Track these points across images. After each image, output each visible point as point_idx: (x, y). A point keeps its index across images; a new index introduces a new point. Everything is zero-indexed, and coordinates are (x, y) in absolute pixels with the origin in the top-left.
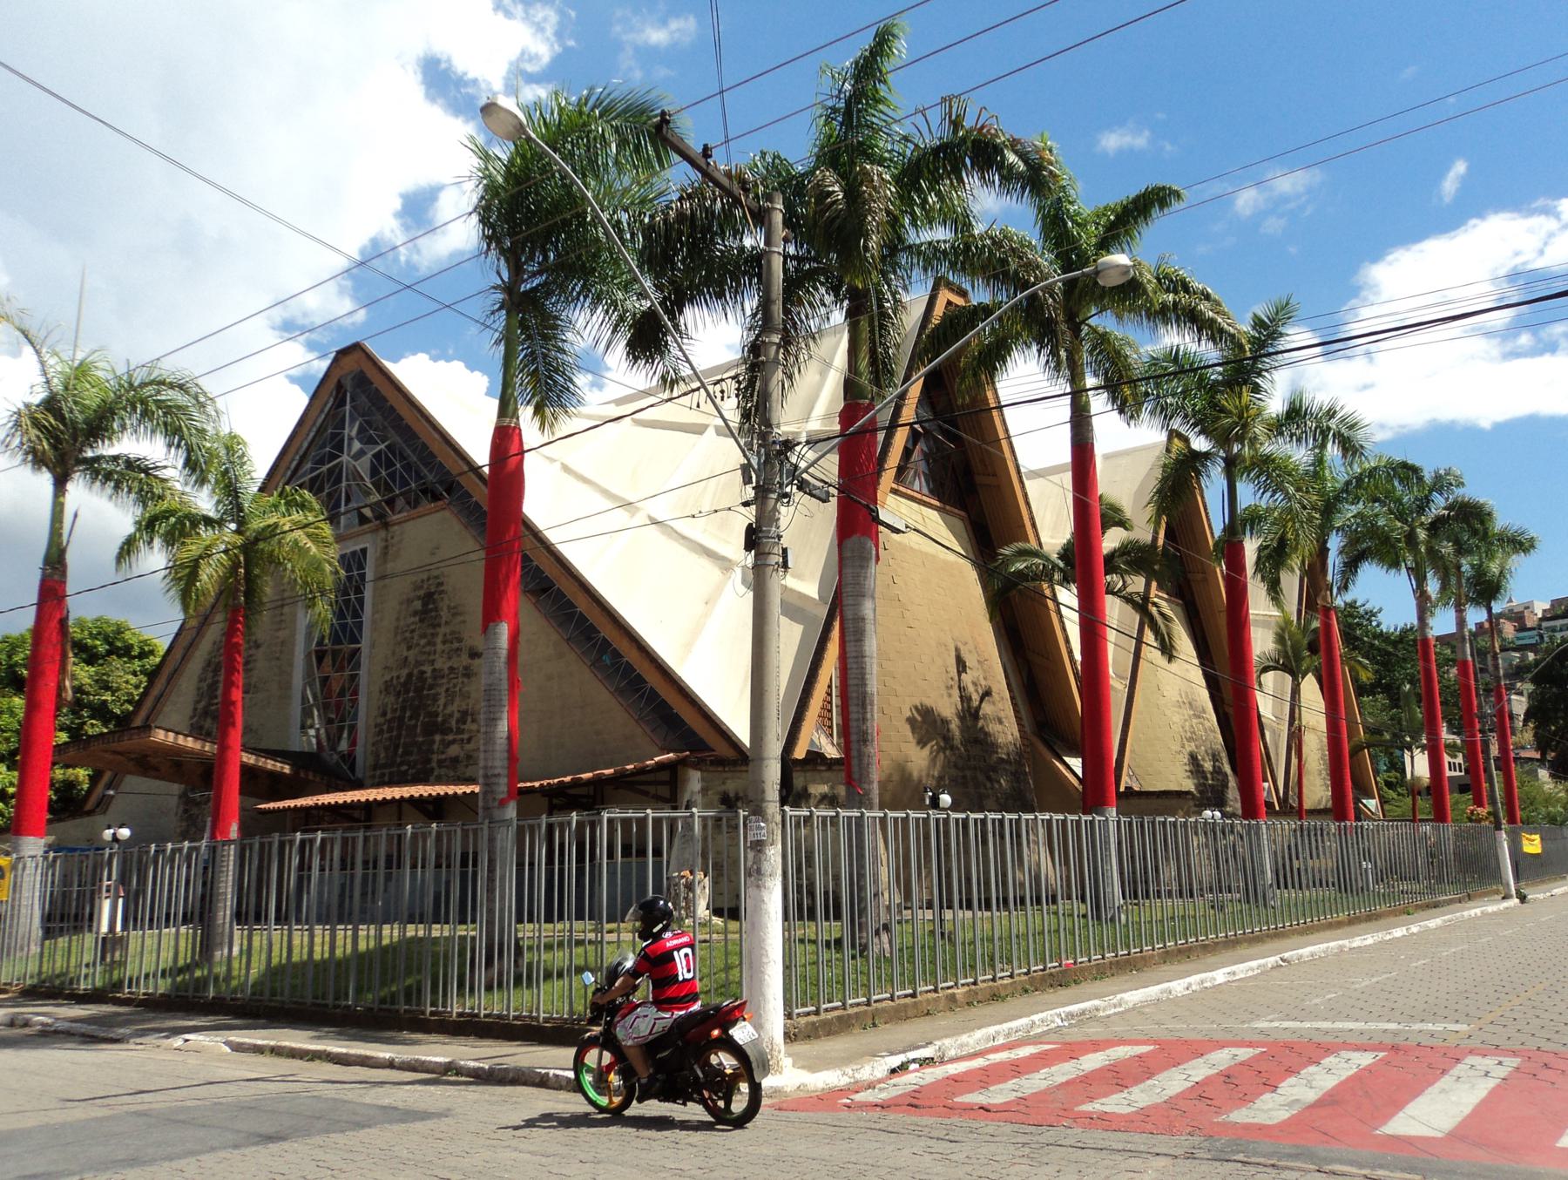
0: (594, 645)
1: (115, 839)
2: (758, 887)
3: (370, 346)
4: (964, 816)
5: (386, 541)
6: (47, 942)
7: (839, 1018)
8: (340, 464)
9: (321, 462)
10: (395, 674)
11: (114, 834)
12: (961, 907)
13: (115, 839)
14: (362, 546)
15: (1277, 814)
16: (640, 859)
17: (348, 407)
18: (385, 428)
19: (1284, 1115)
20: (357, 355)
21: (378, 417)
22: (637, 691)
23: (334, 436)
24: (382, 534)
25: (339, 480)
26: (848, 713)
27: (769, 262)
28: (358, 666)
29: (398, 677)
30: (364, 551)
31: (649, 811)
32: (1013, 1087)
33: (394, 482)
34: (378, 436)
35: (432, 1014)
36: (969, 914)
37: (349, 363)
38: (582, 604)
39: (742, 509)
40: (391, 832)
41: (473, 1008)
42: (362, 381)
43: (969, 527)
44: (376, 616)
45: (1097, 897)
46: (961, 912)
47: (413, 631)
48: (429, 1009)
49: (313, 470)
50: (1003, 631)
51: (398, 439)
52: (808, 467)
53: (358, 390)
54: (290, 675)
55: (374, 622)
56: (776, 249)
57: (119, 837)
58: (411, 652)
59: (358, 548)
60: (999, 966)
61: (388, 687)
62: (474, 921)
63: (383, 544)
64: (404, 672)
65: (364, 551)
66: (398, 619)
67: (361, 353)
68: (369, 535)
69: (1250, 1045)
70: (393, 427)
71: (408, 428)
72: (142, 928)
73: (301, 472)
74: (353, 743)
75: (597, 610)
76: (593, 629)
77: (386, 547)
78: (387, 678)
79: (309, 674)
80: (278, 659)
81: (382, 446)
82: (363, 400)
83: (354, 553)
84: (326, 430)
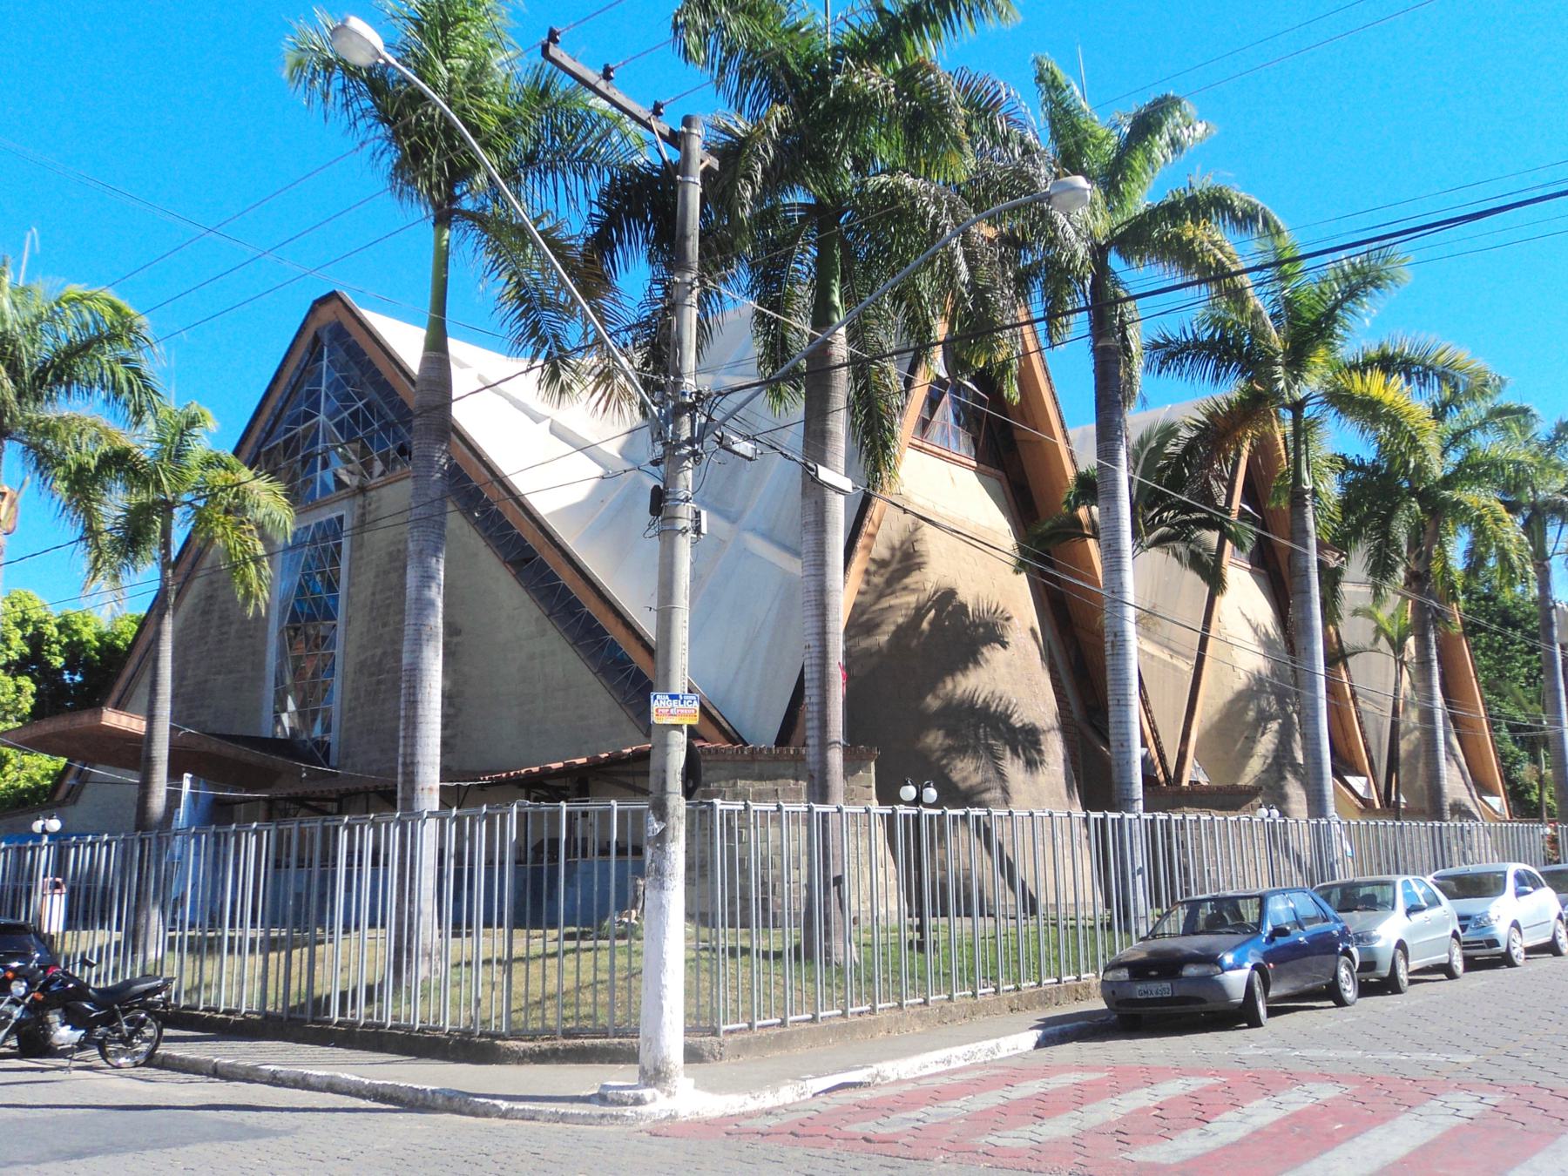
0: (578, 621)
1: (44, 831)
2: (662, 887)
3: (348, 297)
4: (939, 812)
5: (364, 507)
6: (69, 933)
7: (779, 1036)
8: (318, 422)
9: (296, 422)
10: (369, 654)
11: (43, 826)
12: (958, 915)
13: (44, 831)
14: (340, 513)
15: (1376, 814)
16: (637, 858)
17: (325, 362)
18: (362, 383)
19: (1173, 1160)
20: (335, 304)
21: (356, 372)
22: (622, 671)
23: (310, 393)
24: (359, 500)
25: (315, 442)
26: (820, 695)
27: (685, 193)
28: (333, 644)
29: (373, 656)
30: (340, 519)
31: (613, 802)
32: (921, 1116)
33: (372, 443)
34: (356, 394)
35: (339, 1024)
36: (967, 922)
37: (326, 314)
38: (566, 576)
39: (652, 468)
40: (326, 824)
41: (371, 1016)
42: (339, 332)
43: (1007, 489)
44: (352, 590)
45: (1126, 907)
46: (981, 920)
47: (389, 606)
48: (337, 1019)
49: (288, 430)
50: (1046, 605)
51: (377, 397)
52: (726, 419)
53: (335, 344)
54: (263, 653)
55: (349, 596)
56: (692, 179)
57: (48, 828)
58: (387, 629)
59: (334, 515)
60: (980, 981)
61: (361, 667)
62: (383, 926)
63: (361, 511)
64: (379, 651)
65: (340, 519)
66: (373, 594)
67: (339, 303)
68: (345, 501)
69: (1335, 1080)
70: (371, 384)
71: (386, 383)
72: (93, 928)
73: (275, 433)
74: (327, 729)
75: (581, 583)
76: (577, 603)
77: (363, 515)
78: (362, 657)
79: (282, 653)
80: (251, 637)
81: (360, 404)
82: (341, 354)
83: (330, 521)
84: (302, 387)
